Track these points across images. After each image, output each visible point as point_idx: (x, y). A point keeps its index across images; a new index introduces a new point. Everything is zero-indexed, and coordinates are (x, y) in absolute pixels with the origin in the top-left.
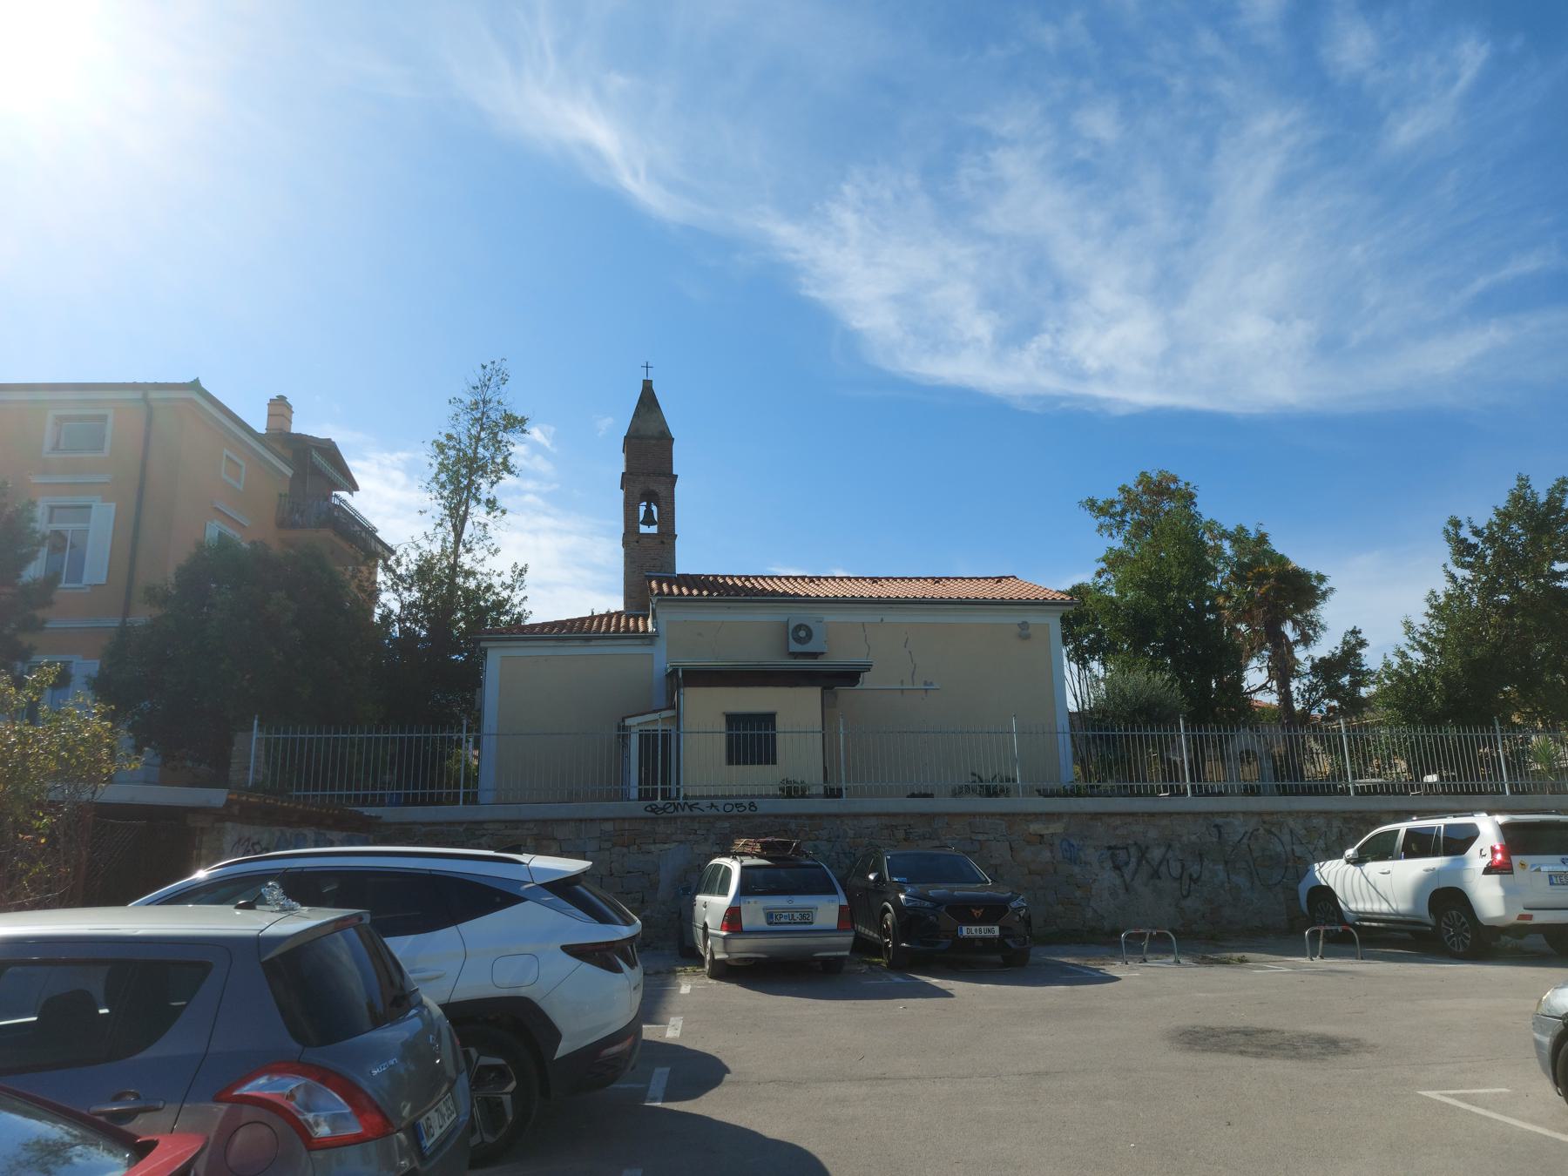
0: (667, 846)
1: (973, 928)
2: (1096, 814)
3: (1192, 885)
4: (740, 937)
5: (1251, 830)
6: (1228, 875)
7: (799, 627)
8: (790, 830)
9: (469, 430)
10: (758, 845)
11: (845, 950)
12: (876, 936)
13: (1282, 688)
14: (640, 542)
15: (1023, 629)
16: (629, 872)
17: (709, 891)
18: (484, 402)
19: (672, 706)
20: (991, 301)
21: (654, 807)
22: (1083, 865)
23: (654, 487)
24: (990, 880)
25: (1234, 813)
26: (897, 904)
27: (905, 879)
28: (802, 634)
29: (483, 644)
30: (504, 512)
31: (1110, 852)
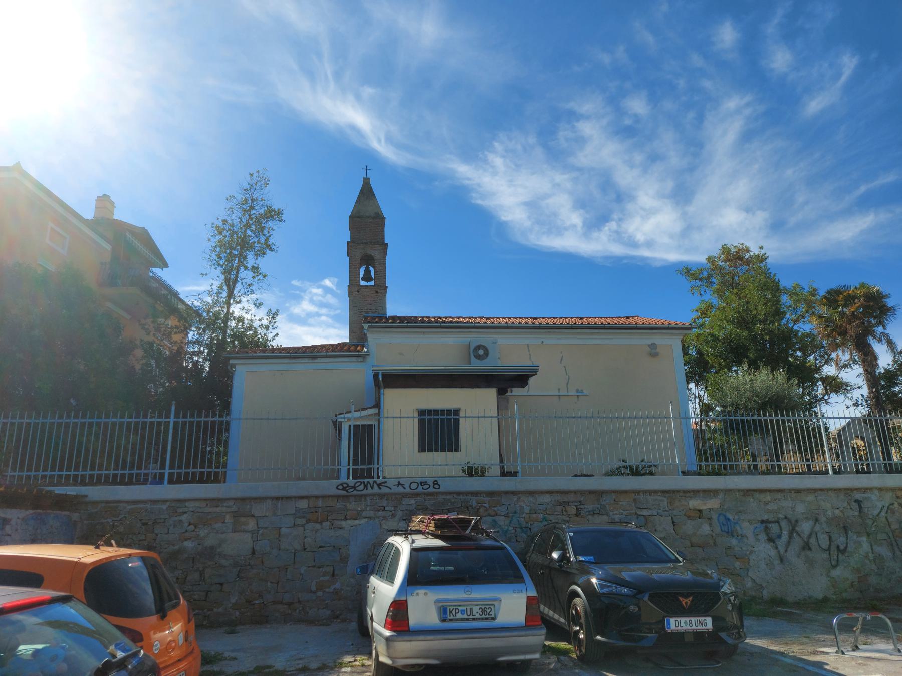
0: (357, 522)
1: (683, 620)
2: (748, 491)
3: (840, 555)
4: (406, 638)
5: (887, 505)
6: (871, 546)
7: (478, 347)
8: (471, 506)
9: (241, 219)
10: (433, 522)
11: (534, 652)
12: (562, 620)
13: (873, 388)
14: (361, 292)
15: (652, 349)
16: (320, 547)
17: (381, 577)
18: (252, 200)
19: (377, 405)
20: (581, 204)
21: (345, 485)
22: (739, 537)
23: (371, 252)
24: (681, 559)
25: (871, 489)
26: (588, 589)
27: (591, 558)
28: (481, 352)
29: (231, 361)
30: (265, 276)
31: (764, 525)
